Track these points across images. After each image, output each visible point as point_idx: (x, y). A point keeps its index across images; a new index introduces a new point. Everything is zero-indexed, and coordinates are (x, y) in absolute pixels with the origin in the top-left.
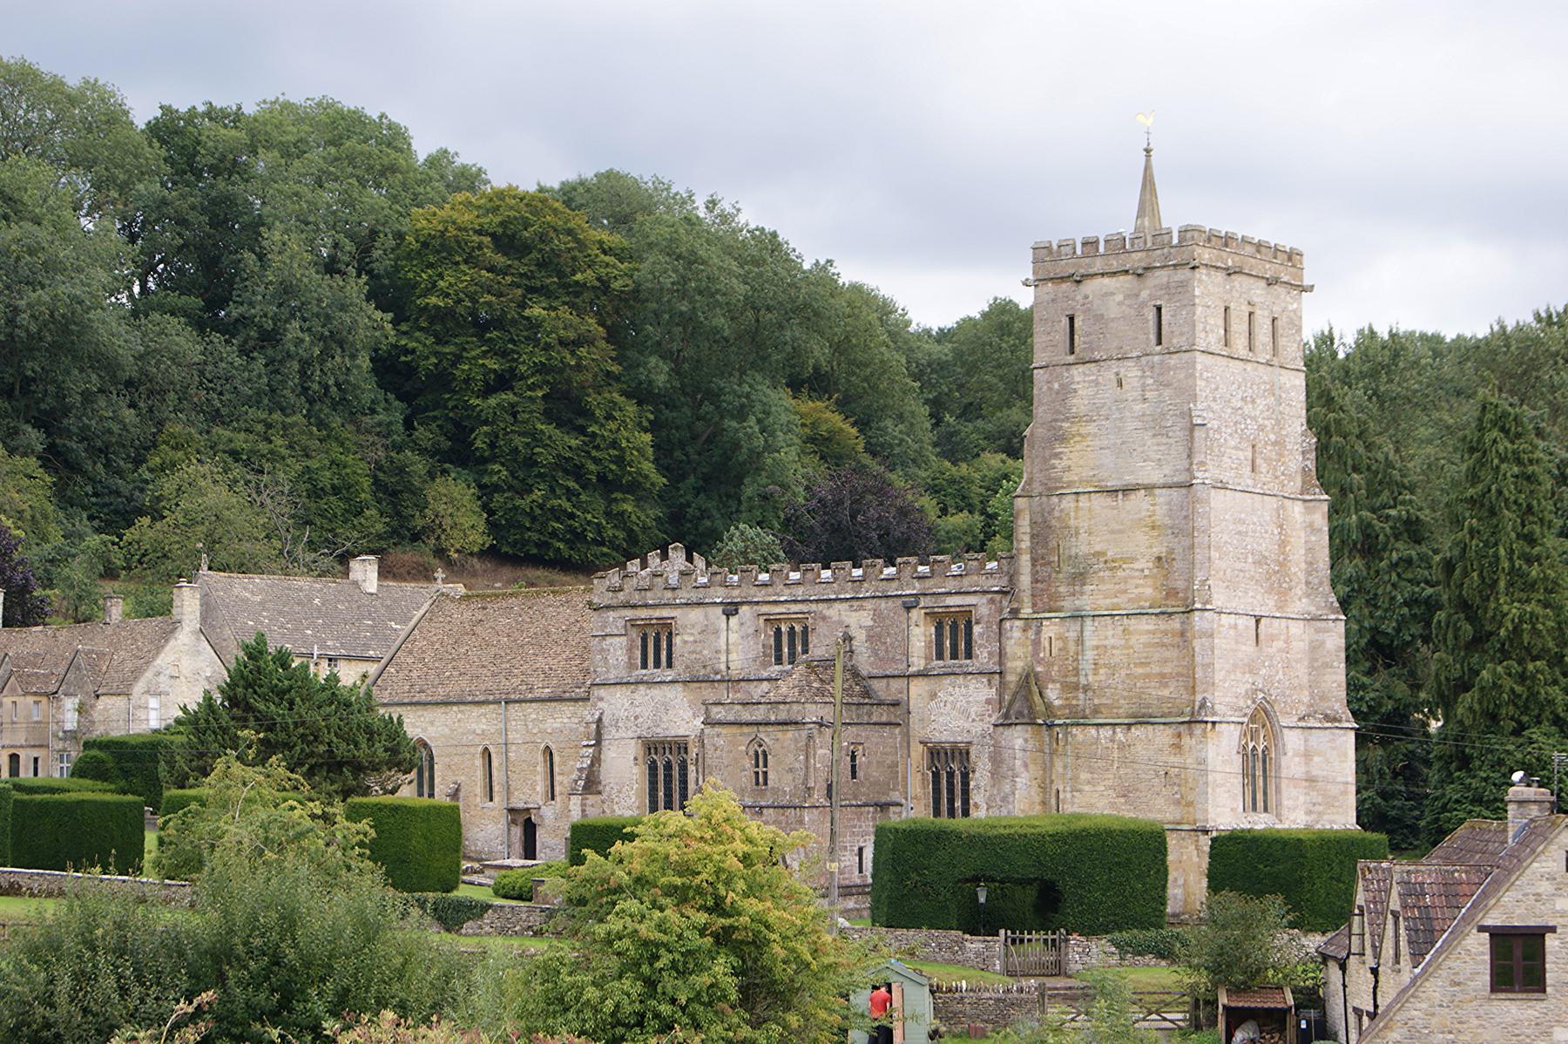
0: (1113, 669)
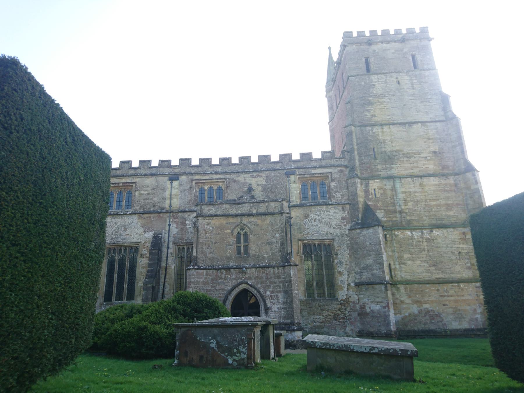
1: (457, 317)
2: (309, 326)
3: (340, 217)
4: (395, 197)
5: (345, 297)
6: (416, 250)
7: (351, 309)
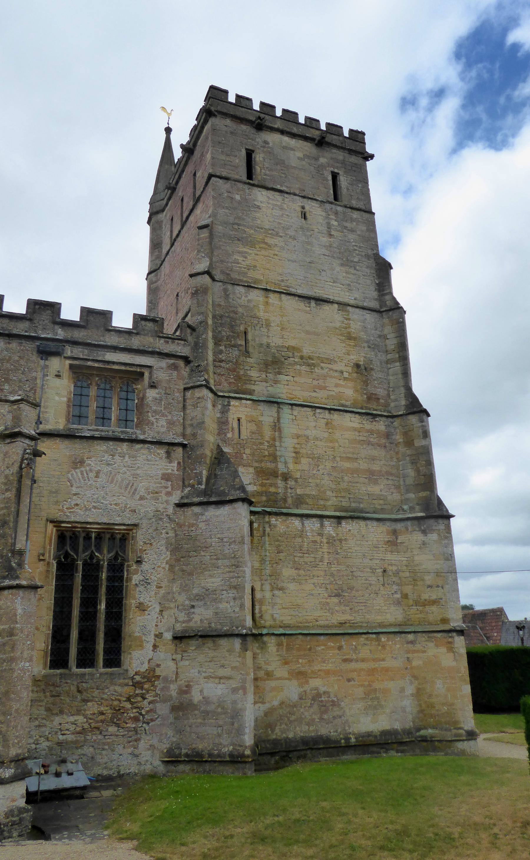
0: (317, 459)
1: (370, 706)
2: (45, 744)
3: (160, 472)
4: (277, 444)
5: (146, 666)
6: (306, 560)
7: (157, 695)
